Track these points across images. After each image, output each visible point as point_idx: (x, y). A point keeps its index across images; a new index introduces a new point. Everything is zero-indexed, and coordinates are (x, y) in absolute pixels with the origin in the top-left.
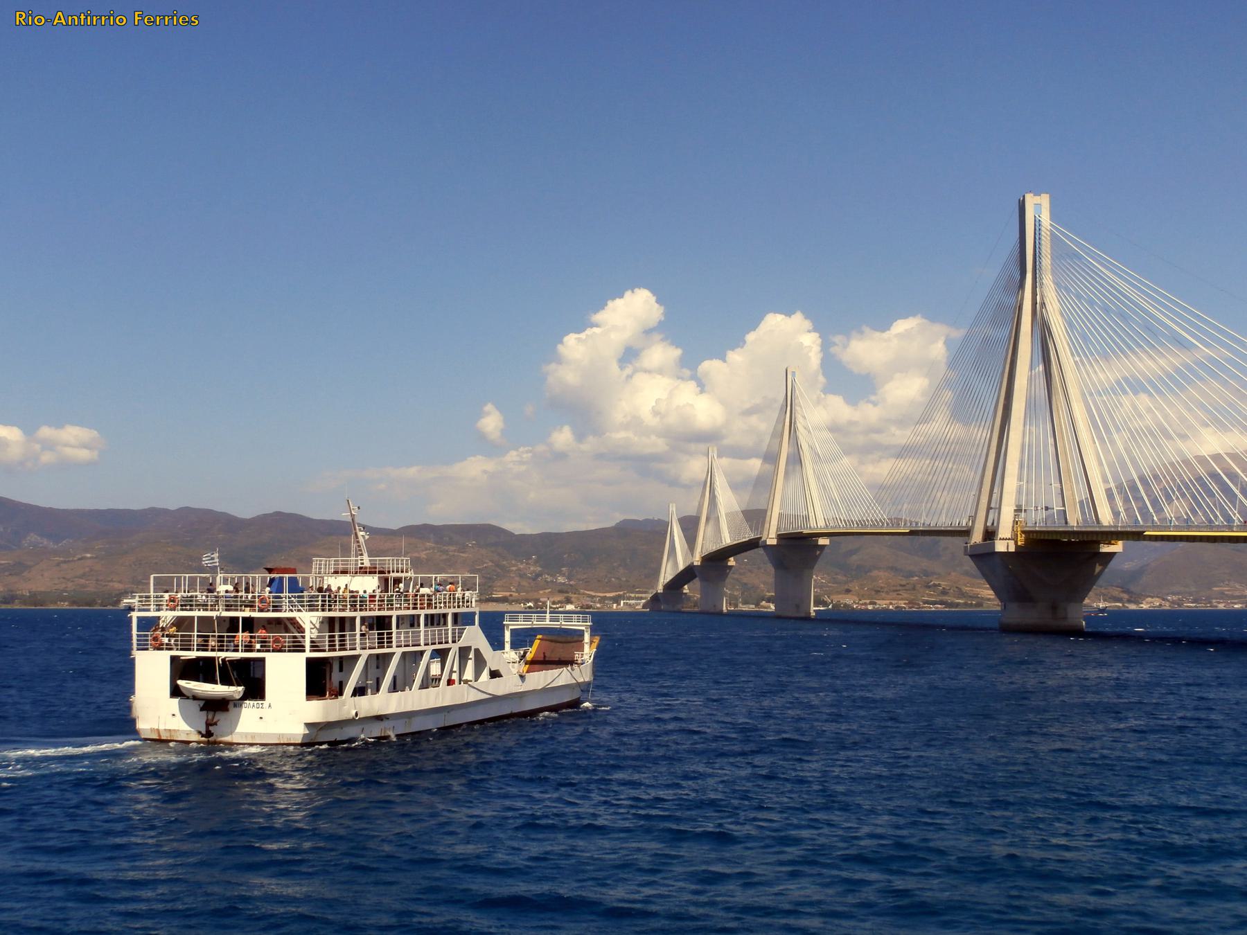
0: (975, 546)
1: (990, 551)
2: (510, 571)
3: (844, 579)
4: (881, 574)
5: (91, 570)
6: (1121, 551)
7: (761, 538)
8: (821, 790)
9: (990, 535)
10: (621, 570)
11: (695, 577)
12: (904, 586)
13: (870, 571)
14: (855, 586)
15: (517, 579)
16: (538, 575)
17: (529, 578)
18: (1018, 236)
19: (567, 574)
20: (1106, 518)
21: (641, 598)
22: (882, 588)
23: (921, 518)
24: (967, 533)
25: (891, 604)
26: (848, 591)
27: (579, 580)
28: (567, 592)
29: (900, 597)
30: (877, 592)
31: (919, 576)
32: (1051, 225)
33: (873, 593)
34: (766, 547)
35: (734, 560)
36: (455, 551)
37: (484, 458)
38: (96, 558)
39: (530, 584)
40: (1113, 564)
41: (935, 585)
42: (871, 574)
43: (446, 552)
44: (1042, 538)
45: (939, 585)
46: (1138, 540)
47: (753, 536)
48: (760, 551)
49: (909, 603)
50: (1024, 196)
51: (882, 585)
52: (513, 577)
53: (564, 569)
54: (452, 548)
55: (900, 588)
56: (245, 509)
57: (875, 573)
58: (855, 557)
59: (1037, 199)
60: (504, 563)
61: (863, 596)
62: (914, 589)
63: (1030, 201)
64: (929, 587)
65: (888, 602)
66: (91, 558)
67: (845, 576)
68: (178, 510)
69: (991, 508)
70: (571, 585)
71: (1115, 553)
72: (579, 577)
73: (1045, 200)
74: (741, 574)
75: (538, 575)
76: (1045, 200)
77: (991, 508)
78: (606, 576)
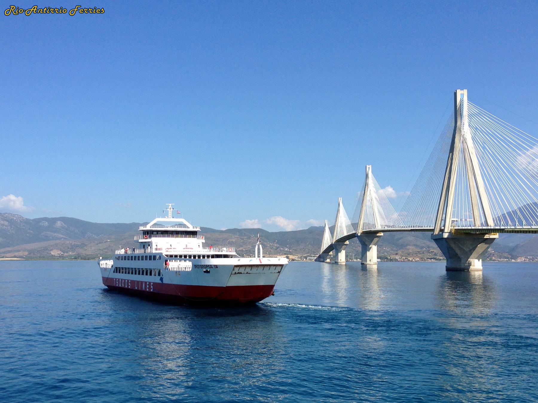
0: (436, 235)
1: (442, 237)
2: (267, 246)
3: (396, 249)
4: (411, 247)
5: (109, 246)
6: (498, 238)
7: (356, 233)
8: (243, 242)
9: (442, 231)
10: (310, 246)
11: (334, 249)
12: (419, 252)
13: (406, 246)
14: (400, 252)
15: (270, 249)
16: (277, 248)
17: (274, 249)
18: (454, 108)
19: (289, 247)
20: (492, 225)
21: (315, 257)
22: (410, 253)
23: (415, 224)
24: (433, 230)
25: (413, 259)
26: (397, 254)
27: (293, 250)
28: (288, 254)
29: (417, 256)
30: (408, 254)
31: (426, 248)
32: (468, 102)
33: (407, 254)
34: (358, 236)
35: (349, 242)
36: (246, 239)
37: (115, 295)
38: (111, 241)
39: (274, 251)
40: (495, 241)
41: (432, 252)
42: (407, 247)
43: (243, 239)
44: (468, 232)
45: (433, 252)
46: (503, 232)
47: (354, 232)
48: (356, 238)
49: (421, 259)
50: (456, 91)
51: (411, 252)
52: (268, 249)
53: (288, 245)
54: (245, 237)
55: (418, 253)
56: (43, 217)
57: (408, 247)
58: (400, 241)
59: (462, 92)
60: (265, 243)
61: (403, 256)
62: (423, 253)
63: (459, 92)
64: (430, 252)
65: (413, 258)
66: (109, 241)
67: (397, 248)
68: (117, 224)
69: (442, 220)
70: (290, 252)
71: (495, 239)
72: (293, 248)
73: (465, 92)
74: (356, 247)
75: (277, 248)
76: (465, 92)
77: (442, 220)
78: (304, 248)
